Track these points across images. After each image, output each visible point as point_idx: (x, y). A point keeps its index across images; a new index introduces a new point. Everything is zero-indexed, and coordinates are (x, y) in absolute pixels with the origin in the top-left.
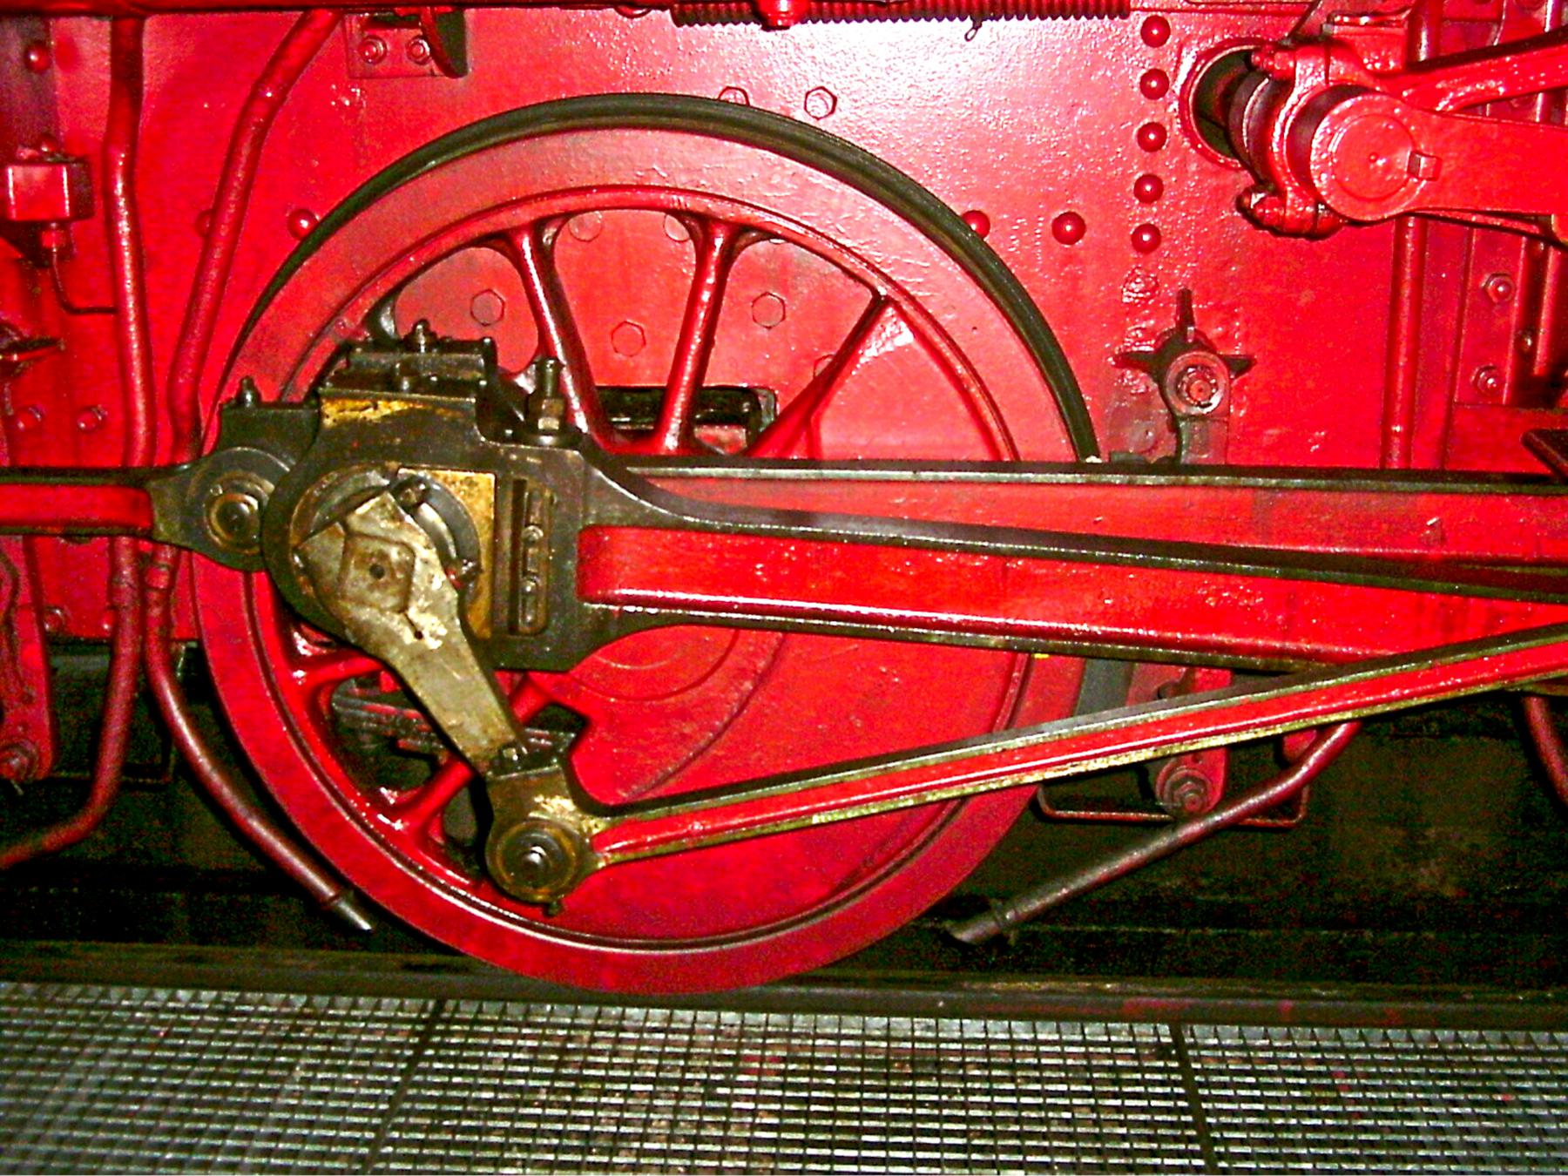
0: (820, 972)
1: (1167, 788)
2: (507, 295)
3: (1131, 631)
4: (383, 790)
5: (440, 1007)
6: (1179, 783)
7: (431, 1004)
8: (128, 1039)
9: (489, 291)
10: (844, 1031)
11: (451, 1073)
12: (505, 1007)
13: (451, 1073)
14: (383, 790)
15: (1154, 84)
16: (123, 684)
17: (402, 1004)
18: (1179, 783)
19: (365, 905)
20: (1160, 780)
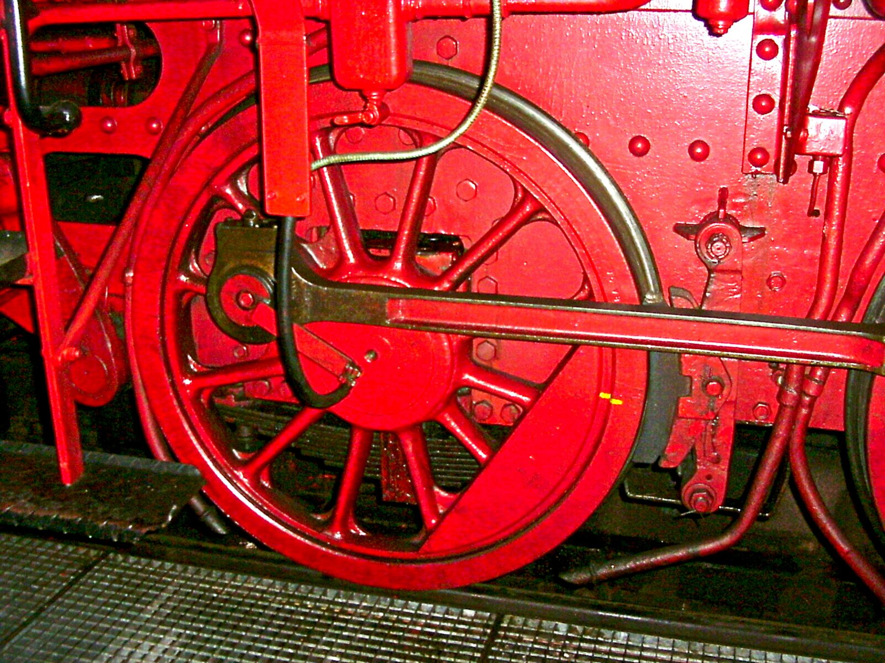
0: (478, 585)
1: (688, 491)
2: (497, 278)
3: (26, 171)
4: (234, 451)
5: (499, 621)
6: (699, 490)
7: (494, 617)
8: (271, 613)
9: (487, 277)
10: (660, 648)
11: (381, 644)
12: (541, 623)
13: (381, 644)
14: (234, 451)
15: (639, 145)
16: (357, 442)
17: (448, 610)
18: (699, 490)
19: (221, 518)
20: (685, 488)
